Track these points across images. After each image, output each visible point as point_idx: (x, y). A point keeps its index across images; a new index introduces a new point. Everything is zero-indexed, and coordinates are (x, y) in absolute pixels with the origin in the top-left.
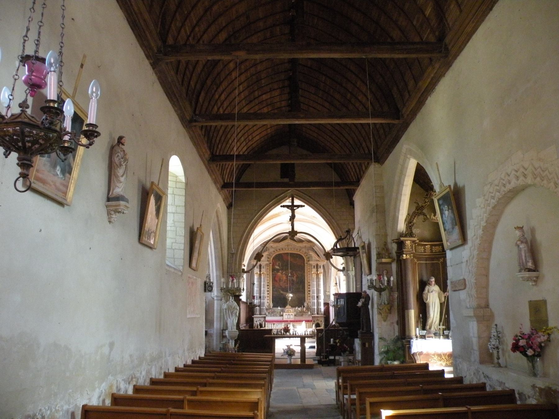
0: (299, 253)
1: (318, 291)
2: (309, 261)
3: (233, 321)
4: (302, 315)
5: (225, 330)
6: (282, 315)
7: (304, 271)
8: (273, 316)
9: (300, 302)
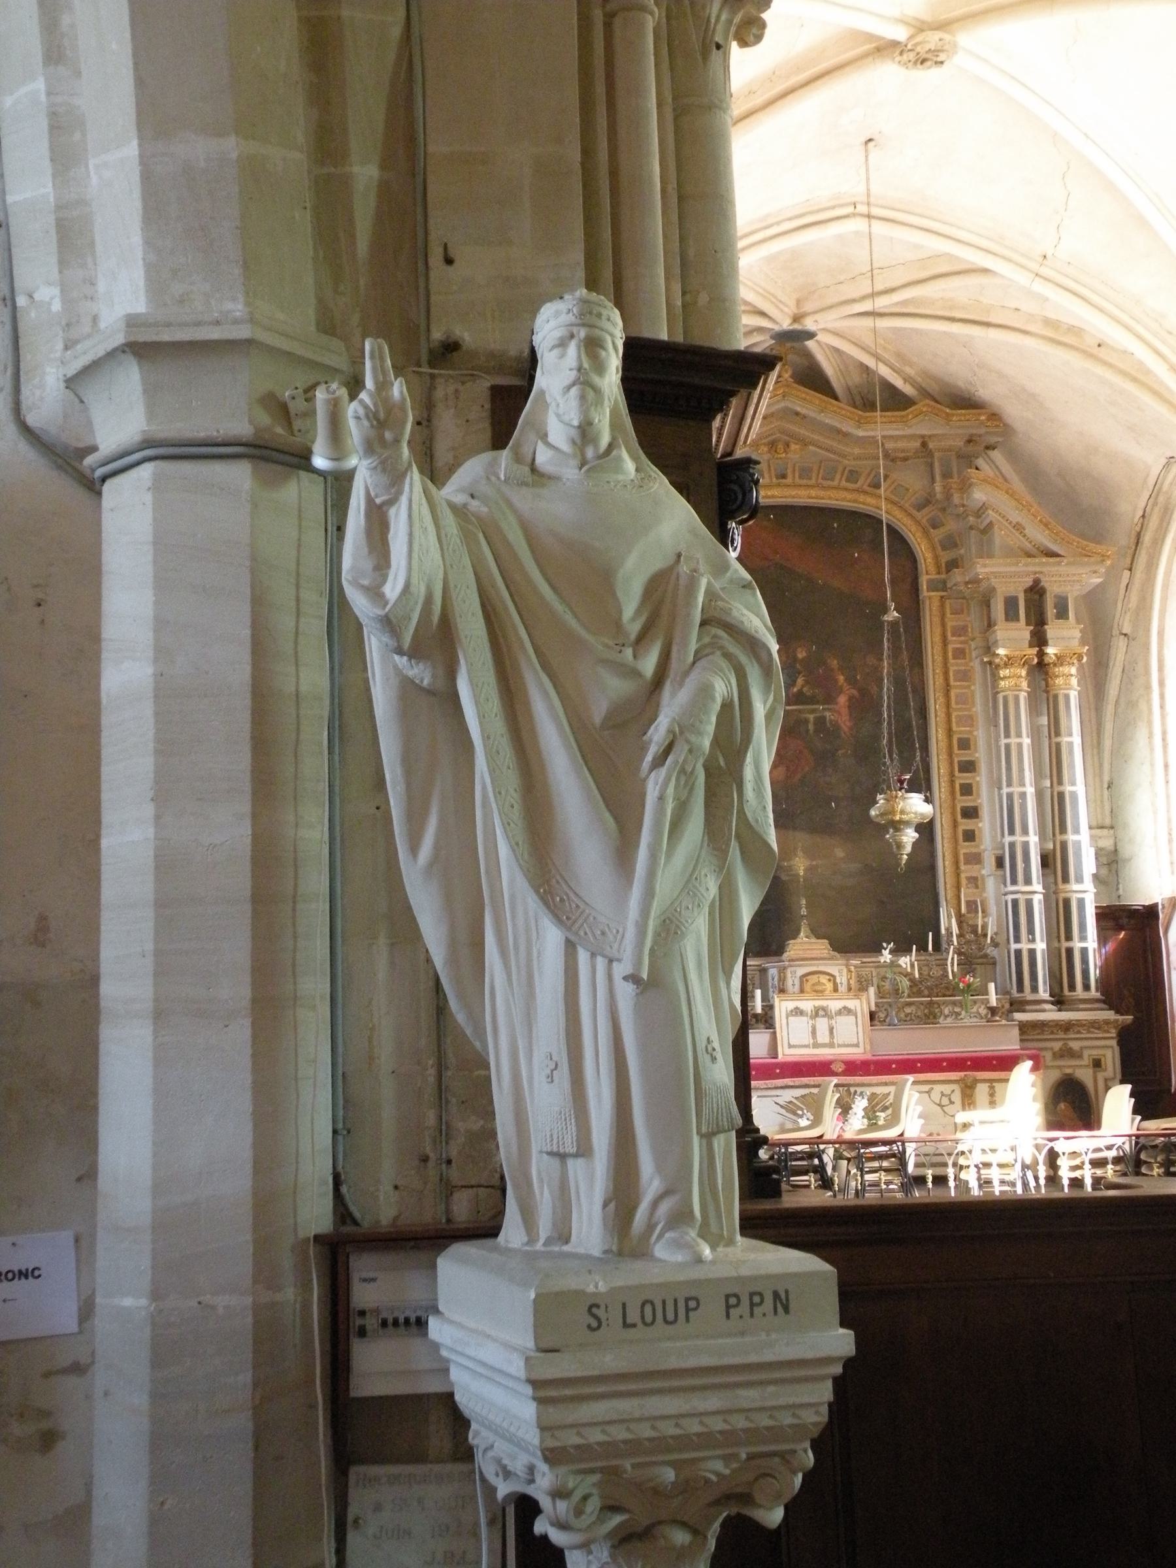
1: (1056, 812)
2: (953, 565)
3: (653, 984)
4: (930, 1016)
5: (425, 1241)
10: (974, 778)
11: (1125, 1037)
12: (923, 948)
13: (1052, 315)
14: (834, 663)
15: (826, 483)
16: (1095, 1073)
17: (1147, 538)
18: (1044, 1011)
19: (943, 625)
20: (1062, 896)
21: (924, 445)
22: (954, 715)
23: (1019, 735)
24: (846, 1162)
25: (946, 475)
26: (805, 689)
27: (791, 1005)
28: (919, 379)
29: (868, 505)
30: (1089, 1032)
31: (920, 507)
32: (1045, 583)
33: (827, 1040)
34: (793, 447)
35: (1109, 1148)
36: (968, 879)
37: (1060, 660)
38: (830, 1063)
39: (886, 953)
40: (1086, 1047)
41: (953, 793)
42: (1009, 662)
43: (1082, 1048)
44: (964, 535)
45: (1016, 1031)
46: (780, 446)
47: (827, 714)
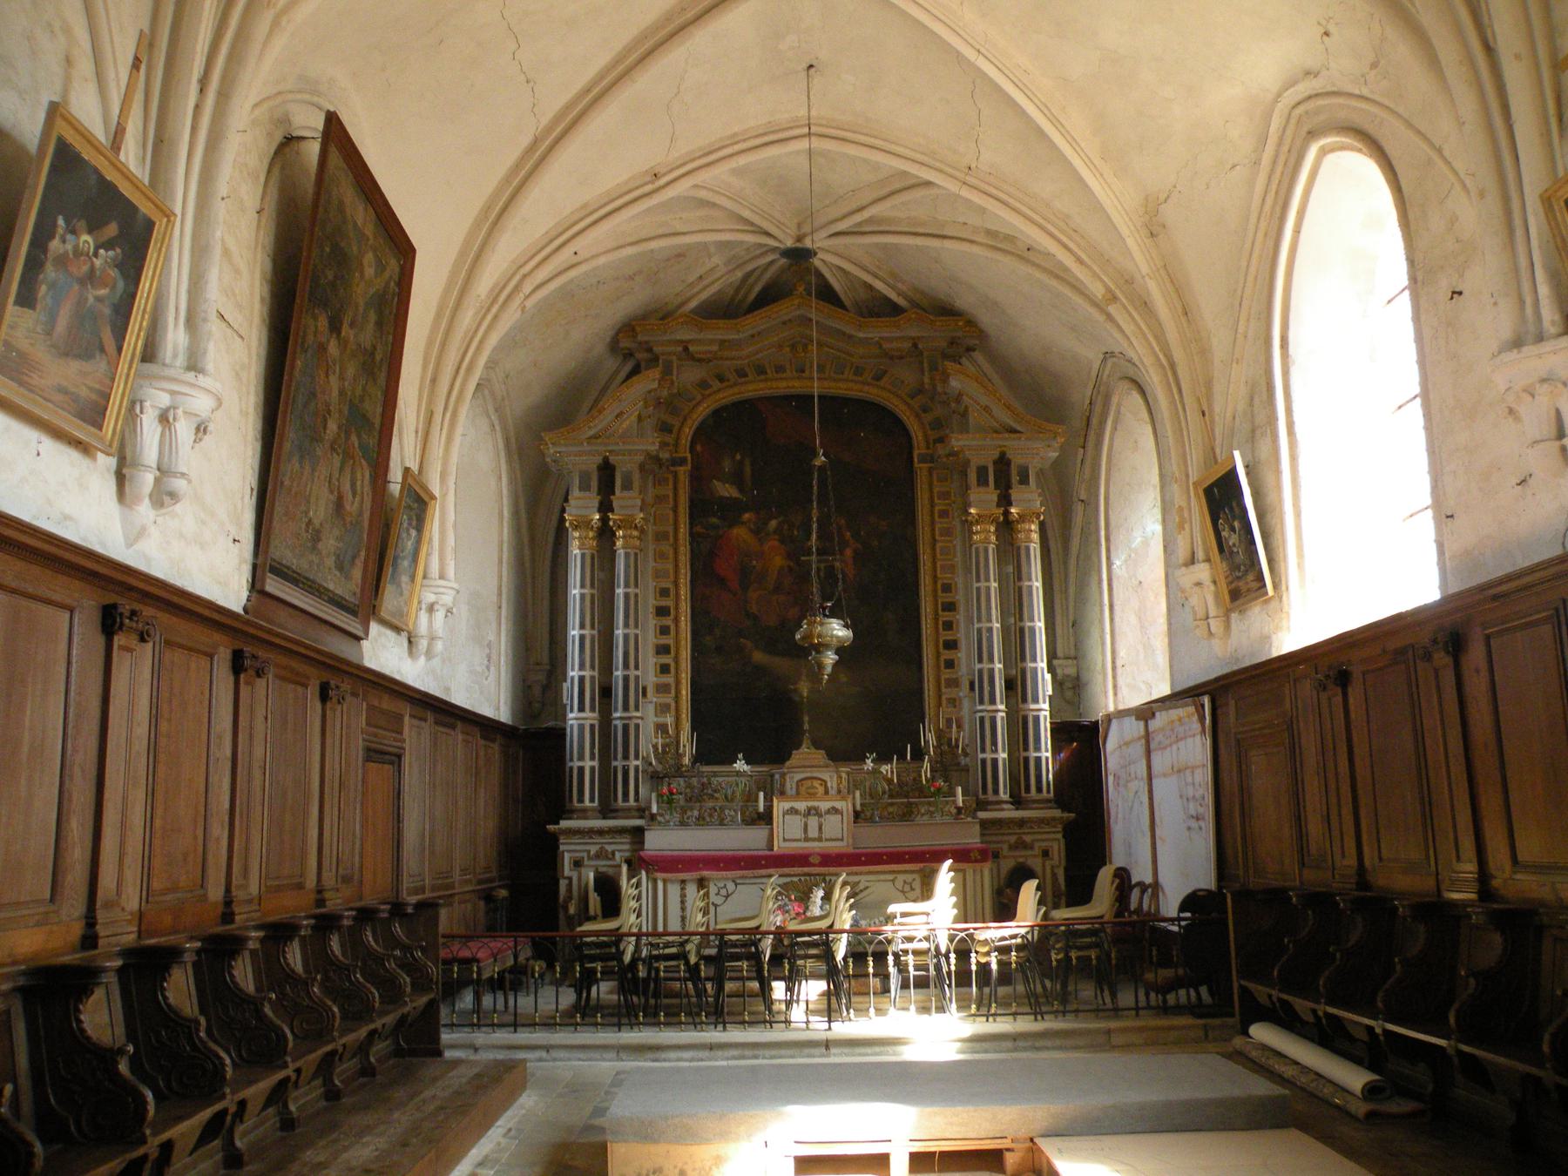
0: (872, 393)
1: (1017, 644)
4: (907, 815)
6: (766, 818)
8: (701, 822)
9: (885, 716)
11: (1069, 831)
12: (902, 757)
13: (989, 226)
17: (1095, 421)
19: (931, 491)
21: (915, 345)
23: (988, 580)
24: (1305, 872)
25: (934, 368)
27: (787, 805)
32: (1010, 455)
33: (816, 835)
35: (1014, 937)
37: (1022, 518)
39: (868, 761)
41: (937, 628)
42: (980, 519)
44: (947, 415)
46: (800, 348)
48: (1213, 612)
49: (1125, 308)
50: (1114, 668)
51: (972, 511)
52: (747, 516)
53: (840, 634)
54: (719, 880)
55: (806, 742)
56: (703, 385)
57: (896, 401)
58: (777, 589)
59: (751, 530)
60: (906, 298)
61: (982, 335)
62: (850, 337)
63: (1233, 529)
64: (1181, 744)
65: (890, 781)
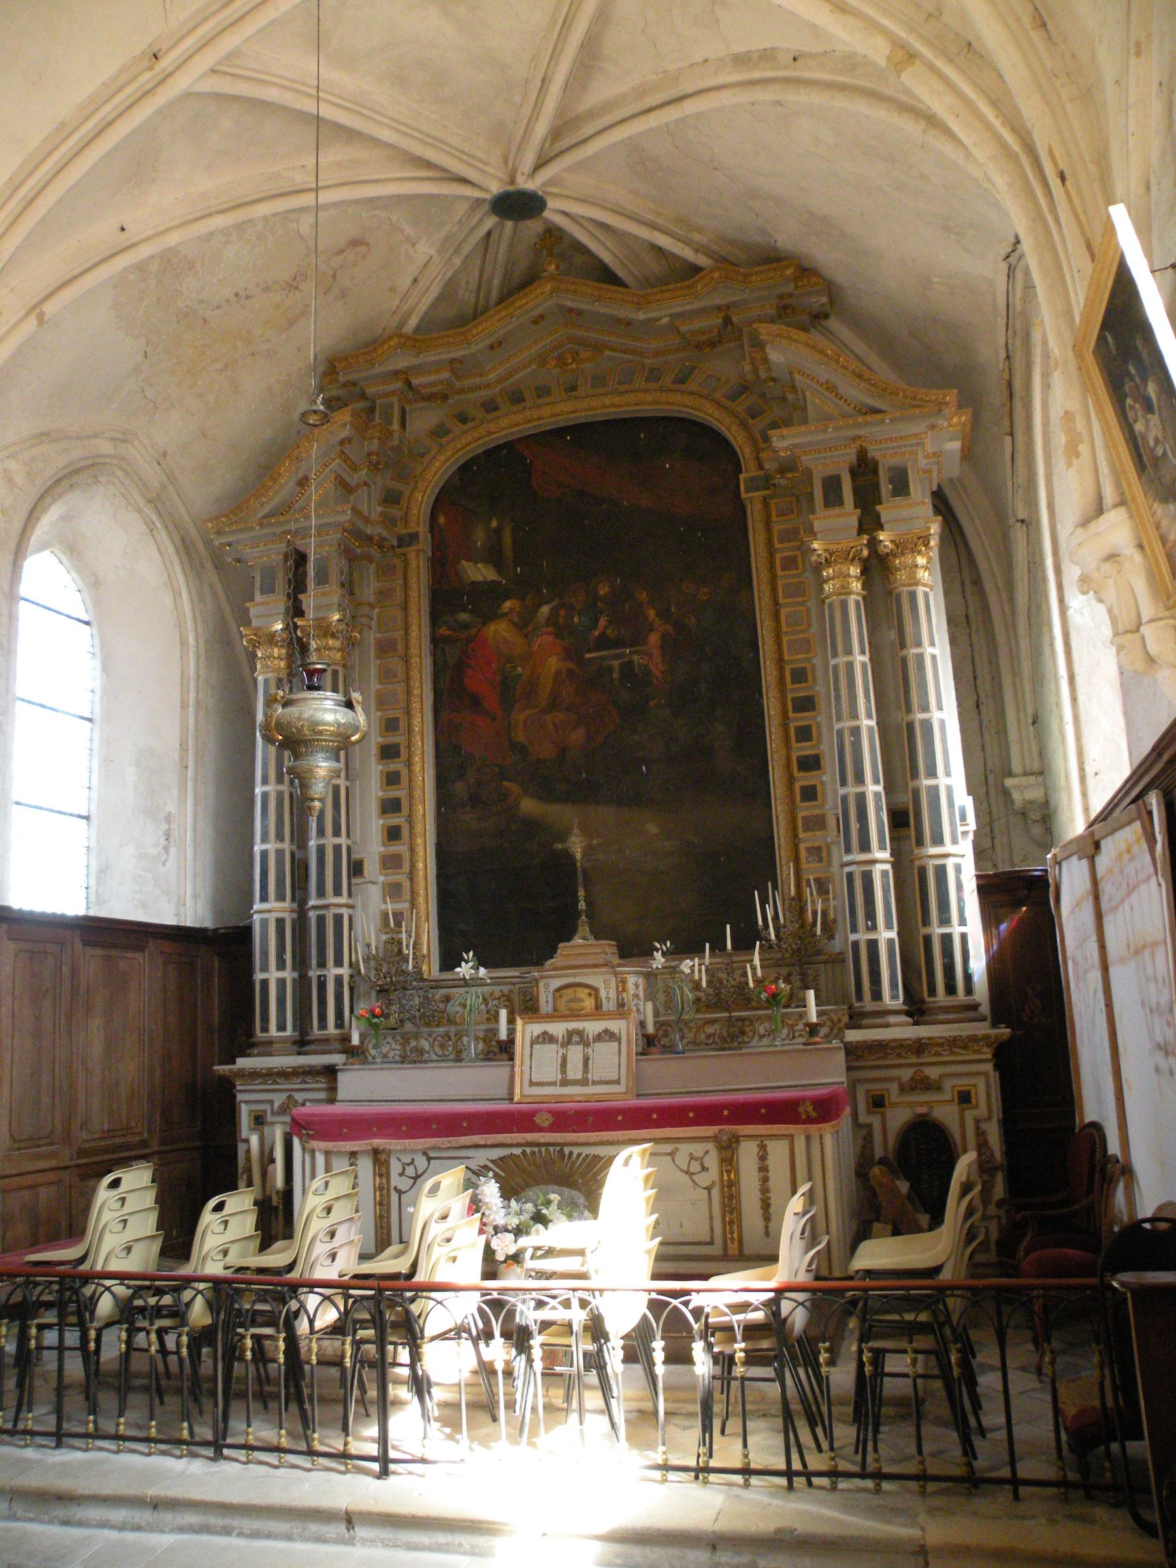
1: (904, 749)
4: (733, 1038)
6: (506, 1049)
7: (746, 579)
9: (719, 891)
10: (814, 718)
11: (1003, 1055)
13: (738, 48)
14: (643, 596)
15: (622, 388)
16: (962, 1111)
17: (1018, 384)
18: (887, 1026)
19: (768, 529)
20: (917, 863)
21: (727, 321)
22: (785, 639)
26: (609, 631)
28: (715, 247)
29: (673, 404)
30: (952, 1053)
31: (734, 397)
32: (874, 452)
33: (579, 1076)
34: (584, 354)
36: (808, 850)
38: (534, 1113)
39: (658, 955)
40: (948, 1075)
43: (941, 1076)
45: (841, 1056)
47: (636, 658)
48: (1148, 610)
49: (932, 68)
50: (1083, 779)
51: (815, 545)
52: (508, 604)
53: (329, 717)
54: (404, 1151)
55: (584, 929)
56: (439, 432)
57: (710, 409)
58: (554, 703)
59: (515, 625)
60: (709, 254)
61: (830, 288)
62: (629, 323)
63: (1149, 408)
64: (1135, 897)
65: (697, 986)
